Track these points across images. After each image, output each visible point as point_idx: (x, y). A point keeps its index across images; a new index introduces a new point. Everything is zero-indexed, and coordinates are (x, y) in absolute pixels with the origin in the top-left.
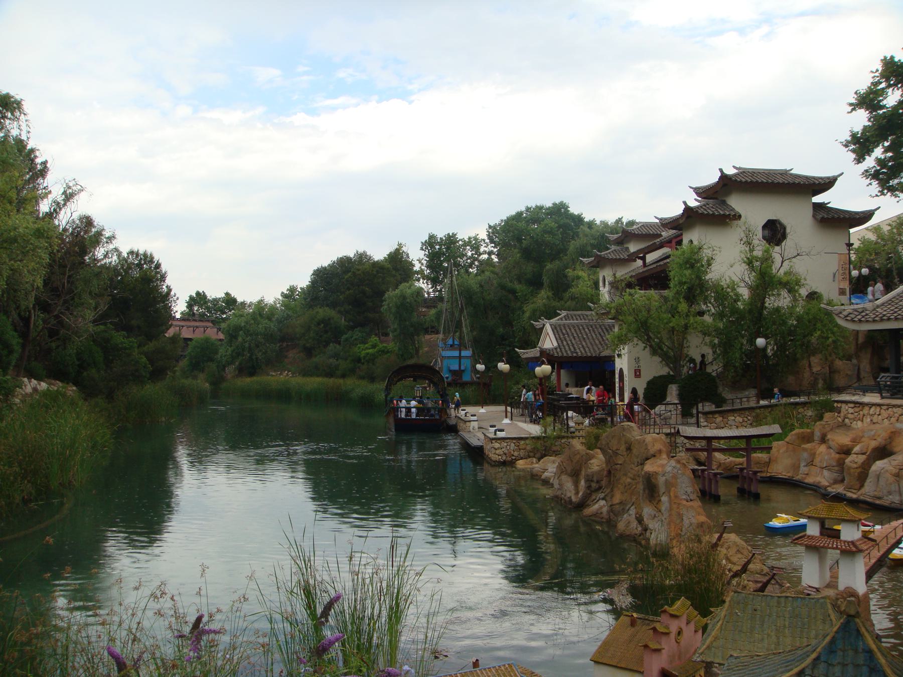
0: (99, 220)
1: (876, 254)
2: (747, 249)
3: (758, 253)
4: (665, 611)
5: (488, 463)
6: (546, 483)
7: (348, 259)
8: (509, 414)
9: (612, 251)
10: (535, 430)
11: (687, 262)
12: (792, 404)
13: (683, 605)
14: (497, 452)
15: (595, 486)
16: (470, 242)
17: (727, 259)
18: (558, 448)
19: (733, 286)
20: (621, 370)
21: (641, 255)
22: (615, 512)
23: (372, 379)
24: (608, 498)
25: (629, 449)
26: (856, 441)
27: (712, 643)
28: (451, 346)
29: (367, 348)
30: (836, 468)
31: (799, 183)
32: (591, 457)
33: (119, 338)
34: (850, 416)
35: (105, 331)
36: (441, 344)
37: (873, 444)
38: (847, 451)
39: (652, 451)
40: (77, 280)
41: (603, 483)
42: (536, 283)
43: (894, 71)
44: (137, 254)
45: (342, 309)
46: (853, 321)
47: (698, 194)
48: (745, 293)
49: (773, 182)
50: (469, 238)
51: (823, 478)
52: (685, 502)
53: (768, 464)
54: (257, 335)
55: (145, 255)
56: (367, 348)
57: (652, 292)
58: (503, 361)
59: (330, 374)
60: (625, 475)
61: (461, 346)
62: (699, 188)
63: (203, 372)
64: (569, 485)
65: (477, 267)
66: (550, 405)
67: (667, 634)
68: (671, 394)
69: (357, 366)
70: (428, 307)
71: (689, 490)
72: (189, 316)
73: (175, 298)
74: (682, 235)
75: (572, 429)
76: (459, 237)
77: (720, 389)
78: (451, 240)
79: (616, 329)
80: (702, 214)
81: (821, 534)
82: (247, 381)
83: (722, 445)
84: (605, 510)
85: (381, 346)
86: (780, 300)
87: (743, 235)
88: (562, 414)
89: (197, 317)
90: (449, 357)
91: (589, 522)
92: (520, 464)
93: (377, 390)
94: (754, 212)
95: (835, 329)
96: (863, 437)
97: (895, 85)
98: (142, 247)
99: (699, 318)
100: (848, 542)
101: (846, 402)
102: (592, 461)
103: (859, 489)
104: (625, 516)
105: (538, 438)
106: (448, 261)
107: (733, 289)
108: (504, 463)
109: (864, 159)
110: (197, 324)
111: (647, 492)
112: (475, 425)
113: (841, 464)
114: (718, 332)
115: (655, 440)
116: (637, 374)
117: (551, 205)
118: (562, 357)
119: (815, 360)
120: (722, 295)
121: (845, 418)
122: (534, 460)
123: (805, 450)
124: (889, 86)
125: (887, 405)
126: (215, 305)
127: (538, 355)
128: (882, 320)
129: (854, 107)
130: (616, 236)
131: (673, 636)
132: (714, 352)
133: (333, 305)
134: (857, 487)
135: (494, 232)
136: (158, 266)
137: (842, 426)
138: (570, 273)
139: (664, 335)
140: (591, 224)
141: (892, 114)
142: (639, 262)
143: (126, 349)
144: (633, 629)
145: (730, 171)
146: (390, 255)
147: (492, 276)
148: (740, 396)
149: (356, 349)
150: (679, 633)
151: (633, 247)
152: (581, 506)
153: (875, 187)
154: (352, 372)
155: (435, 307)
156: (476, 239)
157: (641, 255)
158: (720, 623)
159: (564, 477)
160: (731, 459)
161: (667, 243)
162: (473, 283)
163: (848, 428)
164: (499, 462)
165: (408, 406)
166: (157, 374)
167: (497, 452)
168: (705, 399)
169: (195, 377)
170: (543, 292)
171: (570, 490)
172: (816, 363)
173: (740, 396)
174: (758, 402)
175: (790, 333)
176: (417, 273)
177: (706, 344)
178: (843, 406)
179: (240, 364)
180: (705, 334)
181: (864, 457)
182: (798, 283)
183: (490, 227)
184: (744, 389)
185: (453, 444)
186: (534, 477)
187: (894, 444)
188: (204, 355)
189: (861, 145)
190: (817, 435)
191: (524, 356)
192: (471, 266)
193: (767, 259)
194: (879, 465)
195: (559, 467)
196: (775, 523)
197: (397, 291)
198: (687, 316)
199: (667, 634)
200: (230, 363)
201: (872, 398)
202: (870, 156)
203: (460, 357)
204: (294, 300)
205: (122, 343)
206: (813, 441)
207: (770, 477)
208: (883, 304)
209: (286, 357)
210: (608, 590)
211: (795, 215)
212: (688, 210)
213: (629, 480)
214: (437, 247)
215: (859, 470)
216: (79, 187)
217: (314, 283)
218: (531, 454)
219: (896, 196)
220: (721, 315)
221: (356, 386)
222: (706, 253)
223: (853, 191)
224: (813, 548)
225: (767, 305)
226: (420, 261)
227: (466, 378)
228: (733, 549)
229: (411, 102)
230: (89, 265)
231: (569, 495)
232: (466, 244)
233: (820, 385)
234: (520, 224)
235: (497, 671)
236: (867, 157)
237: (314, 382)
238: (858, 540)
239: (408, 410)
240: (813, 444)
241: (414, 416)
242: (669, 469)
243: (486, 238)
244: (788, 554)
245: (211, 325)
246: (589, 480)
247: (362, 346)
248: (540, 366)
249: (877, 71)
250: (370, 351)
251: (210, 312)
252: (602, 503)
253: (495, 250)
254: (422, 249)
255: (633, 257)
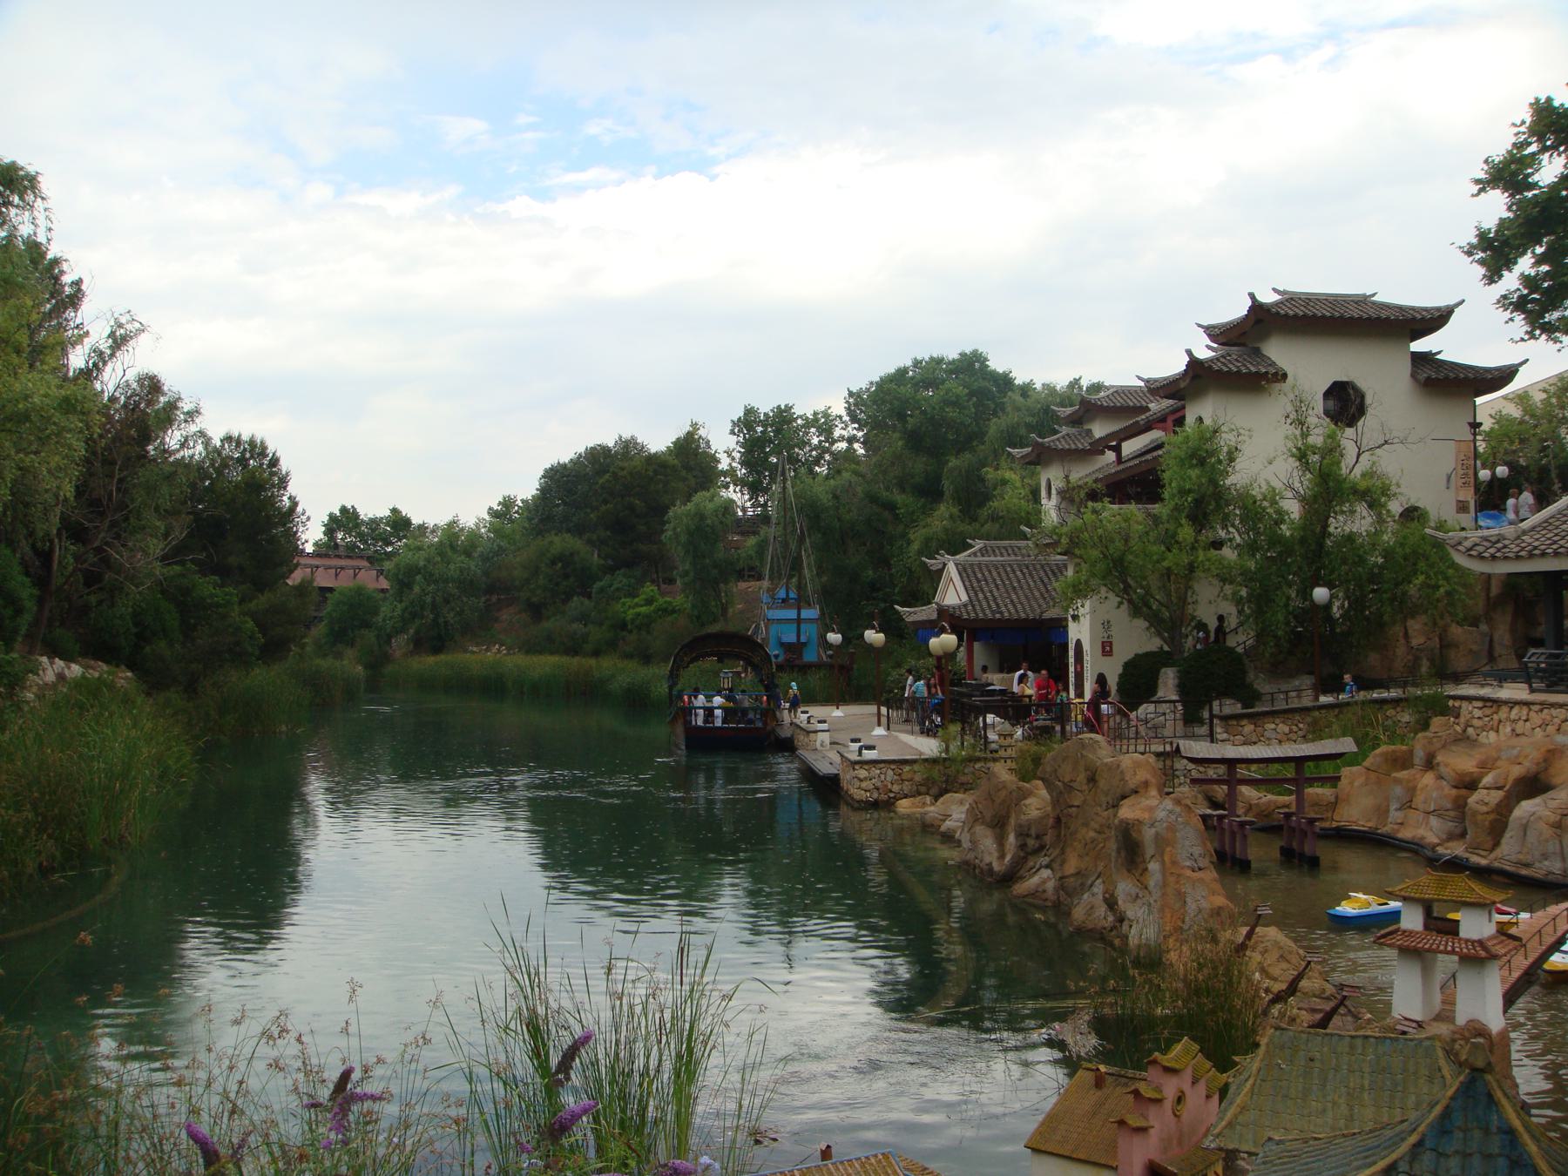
0: (172, 383)
1: (1522, 441)
2: (1298, 432)
3: (1316, 439)
4: (1154, 1062)
5: (848, 804)
6: (949, 838)
7: (605, 450)
8: (884, 720)
9: (1063, 437)
10: (929, 746)
11: (1192, 456)
12: (1375, 701)
13: (1186, 1051)
14: (864, 785)
15: (1033, 845)
16: (816, 420)
17: (1262, 450)
18: (969, 778)
19: (1273, 497)
20: (1079, 643)
21: (1113, 443)
22: (1069, 889)
23: (646, 659)
24: (1055, 866)
25: (1092, 780)
26: (1486, 766)
27: (1236, 1116)
28: (784, 601)
29: (637, 605)
30: (1452, 813)
31: (1387, 319)
32: (1026, 794)
33: (207, 587)
34: (1476, 722)
35: (183, 576)
36: (765, 598)
37: (1517, 771)
38: (1470, 784)
39: (1132, 784)
40: (134, 486)
41: (1048, 839)
42: (930, 492)
43: (1553, 124)
44: (239, 442)
45: (595, 537)
46: (1480, 557)
47: (1212, 337)
48: (1293, 508)
49: (1342, 317)
50: (815, 414)
51: (1429, 831)
52: (1189, 873)
53: (1334, 805)
54: (446, 581)
55: (252, 443)
56: (637, 605)
57: (1132, 508)
58: (873, 627)
59: (573, 650)
60: (1086, 825)
61: (801, 602)
62: (1214, 327)
63: (352, 645)
64: (988, 843)
65: (829, 463)
66: (955, 704)
67: (1159, 1101)
68: (1166, 684)
69: (621, 636)
70: (742, 534)
71: (1197, 851)
72: (327, 549)
73: (304, 518)
74: (1183, 407)
75: (994, 746)
76: (797, 411)
77: (1251, 676)
78: (783, 417)
79: (1070, 572)
80: (1220, 371)
81: (1426, 927)
82: (429, 662)
83: (1254, 772)
84: (1050, 885)
85: (661, 601)
86: (1355, 522)
87: (1290, 408)
88: (977, 719)
89: (341, 551)
90: (779, 621)
91: (1023, 906)
92: (904, 806)
93: (655, 677)
94: (1310, 368)
95: (1451, 571)
96: (1498, 758)
97: (1554, 147)
98: (246, 429)
99: (1213, 552)
100: (1473, 942)
101: (1469, 699)
102: (1027, 802)
103: (1492, 850)
104: (1085, 896)
105: (934, 761)
106: (778, 453)
107: (1274, 502)
108: (875, 805)
109: (1500, 277)
110: (343, 562)
111: (1123, 854)
112: (824, 738)
113: (1460, 806)
114: (1248, 577)
115: (1137, 765)
116: (1107, 649)
117: (956, 356)
118: (976, 620)
119: (1415, 625)
120: (1254, 512)
121: (1468, 725)
122: (928, 799)
123: (1397, 781)
124: (1544, 149)
125: (1541, 704)
126: (373, 530)
127: (934, 616)
128: (1531, 556)
129: (1484, 185)
130: (1069, 410)
131: (1168, 1104)
132: (1240, 612)
133: (579, 530)
134: (1489, 845)
135: (857, 402)
136: (275, 462)
137: (1463, 739)
138: (990, 473)
139: (1154, 581)
140: (1026, 390)
141: (1550, 199)
142: (1110, 456)
143: (218, 605)
144: (1099, 1093)
145: (1268, 297)
146: (677, 443)
147: (854, 479)
148: (1284, 687)
149: (618, 607)
150: (1180, 1099)
151: (1099, 430)
152: (1009, 878)
153: (1519, 324)
154: (611, 646)
155: (755, 533)
156: (826, 415)
157: (1113, 443)
158: (1251, 1082)
159: (980, 829)
160: (1270, 797)
161: (1159, 421)
162: (821, 492)
163: (1472, 743)
164: (867, 802)
165: (708, 706)
166: (273, 649)
167: (864, 785)
168: (1224, 693)
169: (339, 656)
170: (942, 507)
171: (990, 852)
172: (1418, 631)
173: (1284, 687)
174: (1317, 699)
175: (1373, 578)
176: (725, 473)
177: (1225, 598)
178: (1465, 704)
179: (417, 632)
180: (1224, 580)
181: (1501, 793)
182: (1385, 491)
183: (851, 394)
184: (1292, 676)
185: (786, 771)
186: (928, 828)
187: (1552, 771)
188: (354, 617)
189: (1495, 252)
190: (1419, 755)
191: (910, 619)
192: (817, 462)
193: (1332, 450)
194: (1526, 807)
195: (970, 811)
196: (1346, 908)
197: (690, 506)
198: (1193, 548)
199: (1159, 1101)
200: (399, 631)
201: (1514, 691)
202: (1510, 271)
203: (799, 621)
204: (511, 521)
205: (212, 596)
206: (1412, 766)
207: (1338, 829)
208: (1533, 529)
209: (497, 620)
210: (1057, 1025)
211: (1380, 374)
212: (1194, 364)
213: (1092, 834)
214: (759, 429)
215: (1492, 817)
216: (137, 325)
217: (544, 491)
218: (923, 789)
219: (1556, 341)
220: (1251, 548)
221: (619, 671)
222: (1226, 439)
223: (1482, 332)
224: (1413, 952)
225: (1331, 529)
226: (729, 453)
227: (810, 656)
228: (1272, 953)
229: (713, 178)
230: (155, 460)
231: (987, 859)
232: (809, 423)
233: (1424, 669)
234: (903, 390)
235: (863, 1165)
236: (1505, 273)
237: (545, 664)
238: (1490, 939)
239: (709, 712)
240: (1412, 771)
241: (718, 723)
242: (1161, 814)
243: (843, 413)
244: (1368, 963)
245: (366, 564)
246: (1022, 834)
247: (628, 601)
248: (938, 635)
249: (1523, 123)
250: (643, 609)
251: (365, 543)
252: (1046, 873)
253: (860, 434)
254: (732, 432)
255: (1098, 447)
